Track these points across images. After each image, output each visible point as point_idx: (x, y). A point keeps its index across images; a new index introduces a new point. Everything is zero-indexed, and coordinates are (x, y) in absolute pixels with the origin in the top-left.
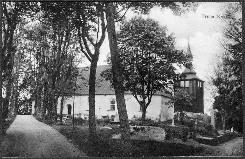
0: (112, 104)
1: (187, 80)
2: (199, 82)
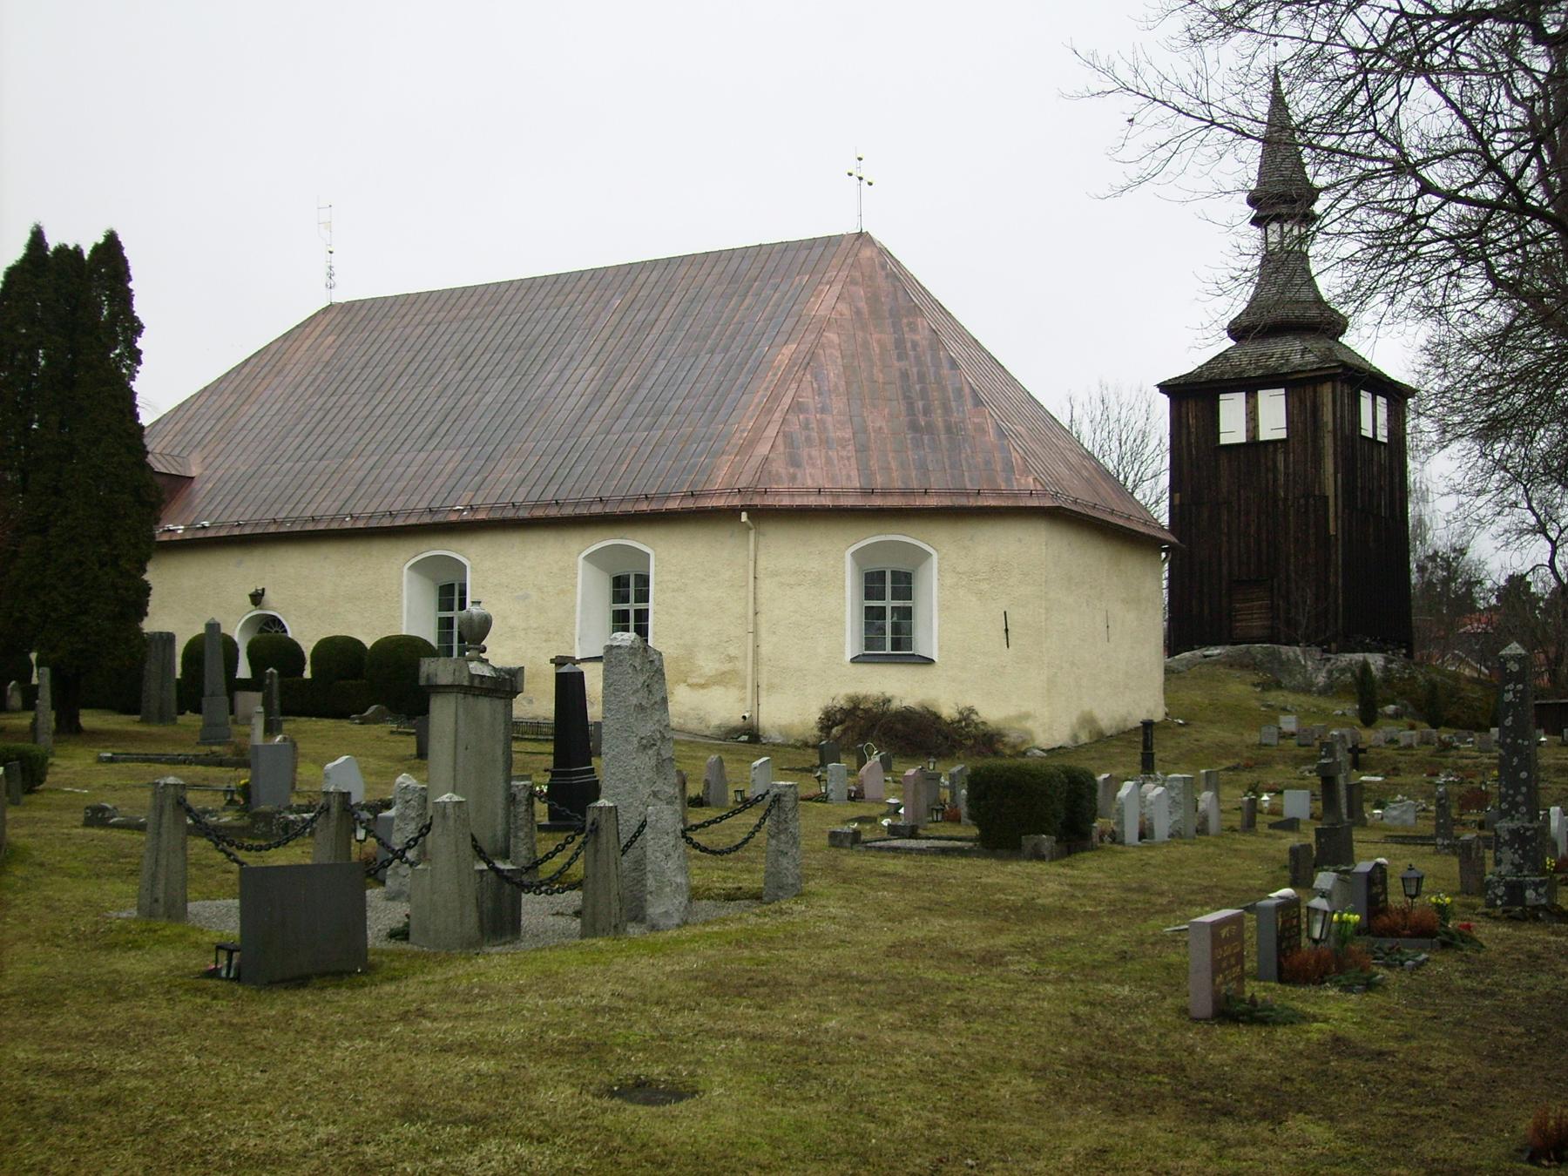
0: (626, 600)
1: (1271, 380)
2: (1366, 400)
